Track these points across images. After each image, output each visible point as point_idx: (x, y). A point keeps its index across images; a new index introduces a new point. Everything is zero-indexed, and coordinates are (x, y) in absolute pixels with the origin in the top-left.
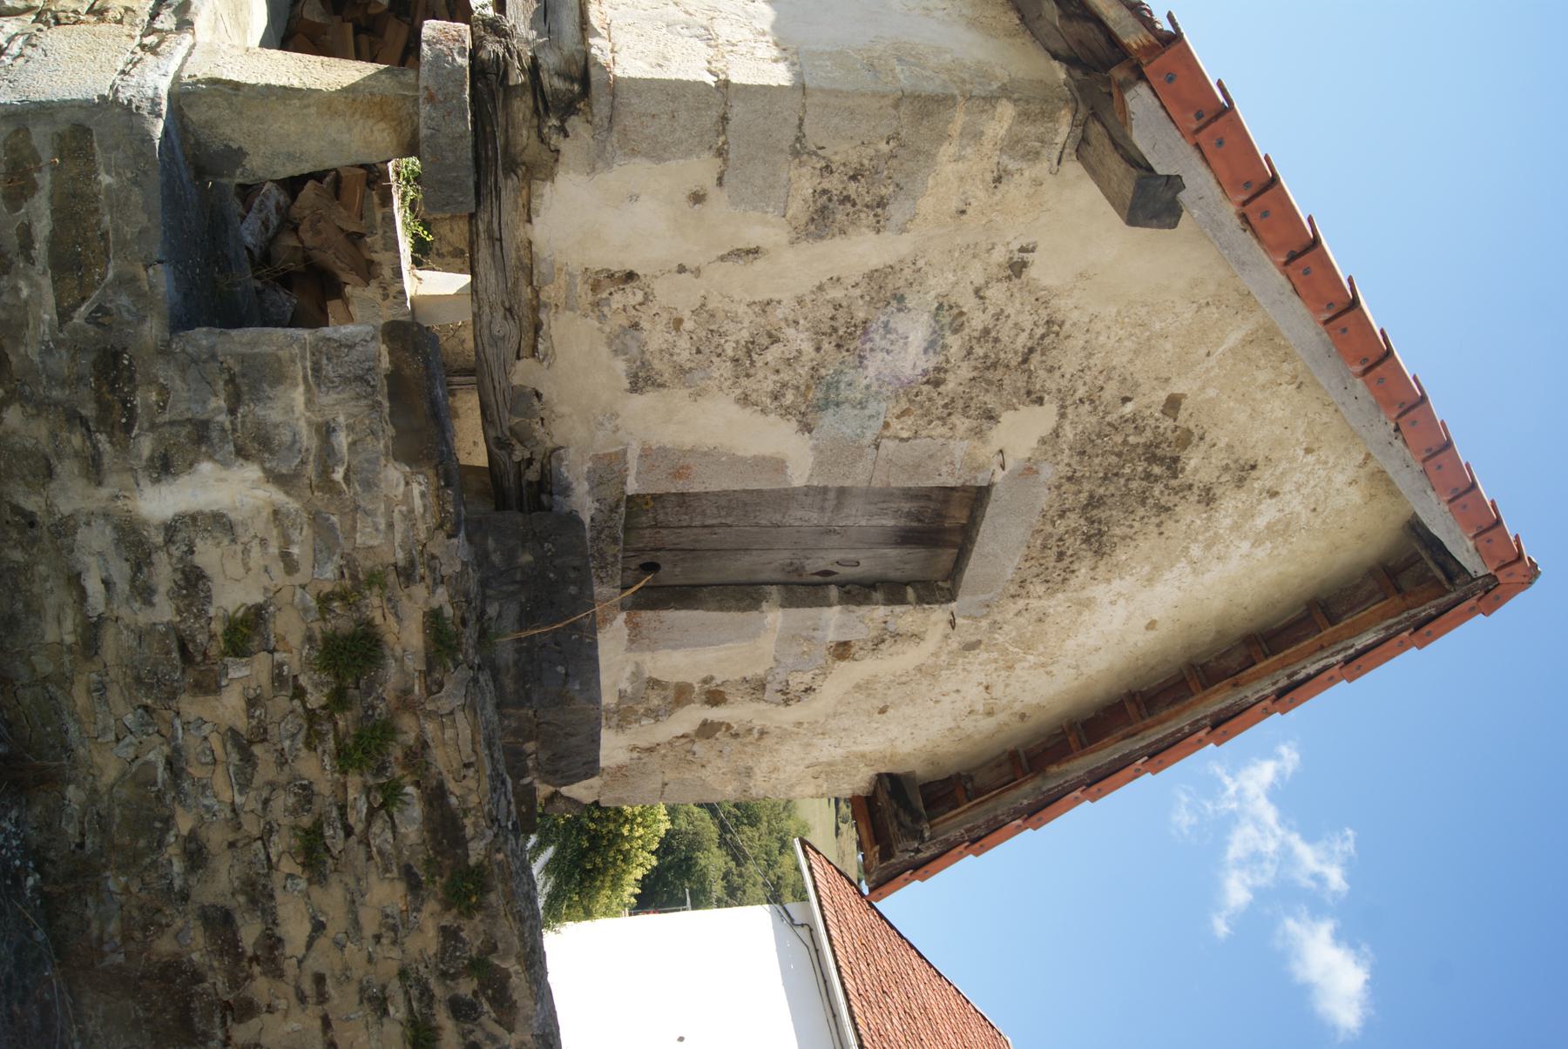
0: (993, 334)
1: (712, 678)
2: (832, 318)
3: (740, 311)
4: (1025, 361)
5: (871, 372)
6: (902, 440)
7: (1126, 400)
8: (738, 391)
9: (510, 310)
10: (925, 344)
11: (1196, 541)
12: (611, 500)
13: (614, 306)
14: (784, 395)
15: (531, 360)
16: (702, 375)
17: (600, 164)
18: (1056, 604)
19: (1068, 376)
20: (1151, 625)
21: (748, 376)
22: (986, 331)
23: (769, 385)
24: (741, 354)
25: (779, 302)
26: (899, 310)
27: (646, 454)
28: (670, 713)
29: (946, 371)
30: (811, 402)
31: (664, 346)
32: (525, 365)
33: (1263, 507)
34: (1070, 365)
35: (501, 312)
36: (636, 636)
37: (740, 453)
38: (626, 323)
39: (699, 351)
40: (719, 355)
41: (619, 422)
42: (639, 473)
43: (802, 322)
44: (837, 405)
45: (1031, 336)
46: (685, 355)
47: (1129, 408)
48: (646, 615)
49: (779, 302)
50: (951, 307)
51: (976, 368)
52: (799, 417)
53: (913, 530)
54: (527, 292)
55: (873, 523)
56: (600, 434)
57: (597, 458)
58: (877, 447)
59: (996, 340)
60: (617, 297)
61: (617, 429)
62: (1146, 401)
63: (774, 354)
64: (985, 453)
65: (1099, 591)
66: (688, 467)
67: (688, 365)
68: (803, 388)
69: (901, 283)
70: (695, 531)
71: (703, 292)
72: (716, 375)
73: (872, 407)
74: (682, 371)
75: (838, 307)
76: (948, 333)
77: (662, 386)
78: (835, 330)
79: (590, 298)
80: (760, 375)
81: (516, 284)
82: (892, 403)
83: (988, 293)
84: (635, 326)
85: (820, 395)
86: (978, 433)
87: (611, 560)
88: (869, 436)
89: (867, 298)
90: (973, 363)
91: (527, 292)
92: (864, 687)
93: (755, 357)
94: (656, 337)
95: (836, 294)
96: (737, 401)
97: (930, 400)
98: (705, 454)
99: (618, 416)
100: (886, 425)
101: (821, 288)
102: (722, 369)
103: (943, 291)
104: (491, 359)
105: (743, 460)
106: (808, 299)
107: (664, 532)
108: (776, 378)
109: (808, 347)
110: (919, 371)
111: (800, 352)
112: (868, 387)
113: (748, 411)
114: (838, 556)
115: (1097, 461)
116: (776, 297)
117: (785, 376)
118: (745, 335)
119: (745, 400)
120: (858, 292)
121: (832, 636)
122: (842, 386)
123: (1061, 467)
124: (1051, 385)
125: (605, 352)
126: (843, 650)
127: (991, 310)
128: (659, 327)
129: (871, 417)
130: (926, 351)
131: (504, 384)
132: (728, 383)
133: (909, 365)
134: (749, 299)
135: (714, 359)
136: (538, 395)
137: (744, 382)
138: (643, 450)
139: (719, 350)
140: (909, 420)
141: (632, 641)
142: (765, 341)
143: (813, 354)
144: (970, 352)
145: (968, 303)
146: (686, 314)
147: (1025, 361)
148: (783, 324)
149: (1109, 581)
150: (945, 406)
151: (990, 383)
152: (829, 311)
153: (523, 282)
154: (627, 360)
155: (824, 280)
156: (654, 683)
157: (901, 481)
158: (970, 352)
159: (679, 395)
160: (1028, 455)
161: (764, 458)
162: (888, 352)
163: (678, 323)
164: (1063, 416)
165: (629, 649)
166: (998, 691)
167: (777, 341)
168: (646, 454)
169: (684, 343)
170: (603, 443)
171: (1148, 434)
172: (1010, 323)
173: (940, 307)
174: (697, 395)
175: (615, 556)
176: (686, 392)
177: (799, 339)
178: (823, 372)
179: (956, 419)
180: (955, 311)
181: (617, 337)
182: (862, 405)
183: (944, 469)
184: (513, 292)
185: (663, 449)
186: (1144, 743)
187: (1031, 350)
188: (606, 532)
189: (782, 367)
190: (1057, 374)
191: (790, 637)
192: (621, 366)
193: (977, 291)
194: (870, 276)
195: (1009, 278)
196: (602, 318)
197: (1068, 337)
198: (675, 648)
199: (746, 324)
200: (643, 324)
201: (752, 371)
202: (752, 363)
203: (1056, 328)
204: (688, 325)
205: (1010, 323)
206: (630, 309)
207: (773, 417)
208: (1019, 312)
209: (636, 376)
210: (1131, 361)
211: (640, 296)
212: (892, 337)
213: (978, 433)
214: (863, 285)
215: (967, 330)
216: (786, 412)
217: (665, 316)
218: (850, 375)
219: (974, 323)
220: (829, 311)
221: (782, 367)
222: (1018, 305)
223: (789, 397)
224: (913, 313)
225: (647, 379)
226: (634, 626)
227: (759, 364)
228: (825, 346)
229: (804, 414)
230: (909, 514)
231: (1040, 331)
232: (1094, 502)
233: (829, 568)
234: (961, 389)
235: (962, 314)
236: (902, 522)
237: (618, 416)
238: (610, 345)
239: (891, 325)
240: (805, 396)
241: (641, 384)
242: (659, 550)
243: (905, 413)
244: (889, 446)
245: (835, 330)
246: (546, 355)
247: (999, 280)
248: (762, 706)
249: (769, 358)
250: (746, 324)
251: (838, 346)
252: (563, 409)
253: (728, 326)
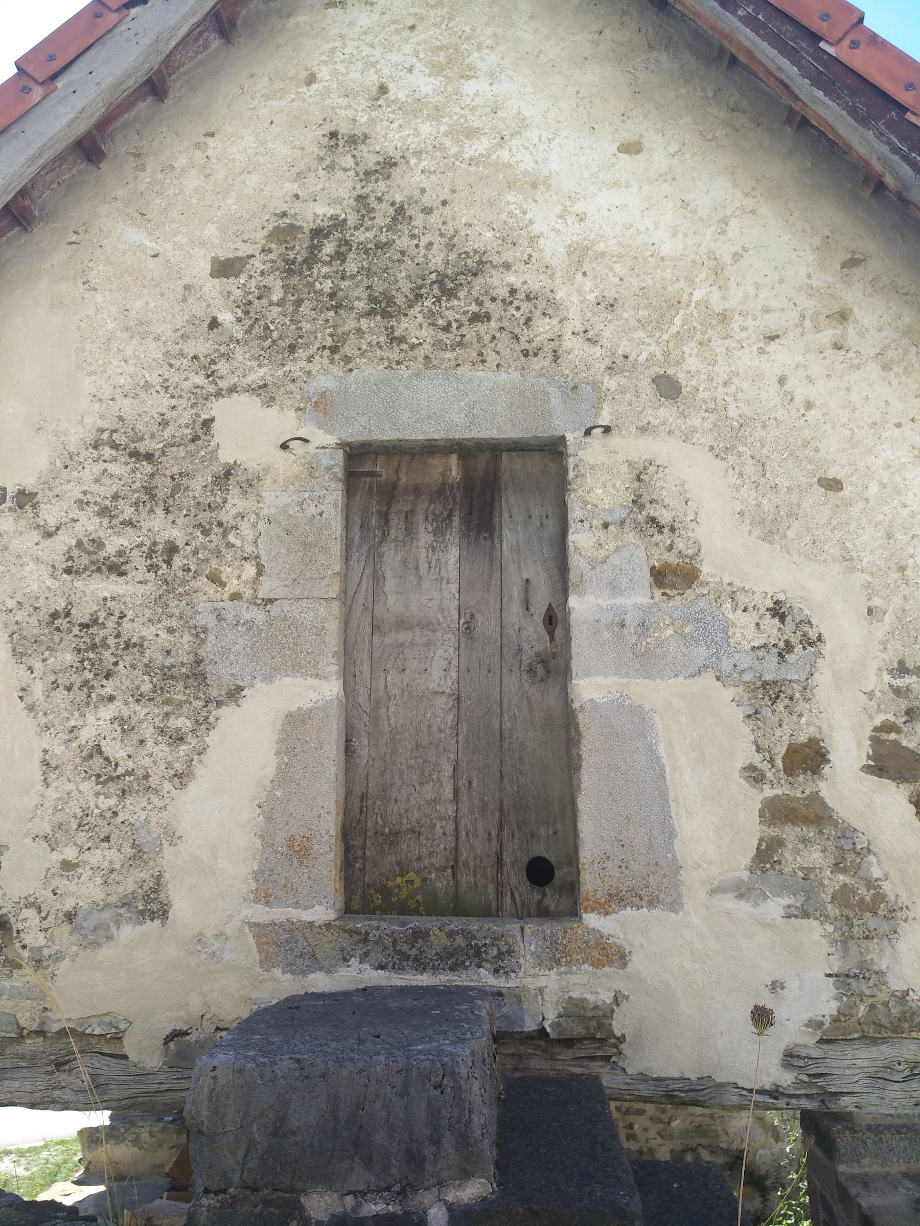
0: (107, 503)
1: (751, 768)
2: (69, 689)
3: (56, 795)
4: (149, 457)
5: (149, 632)
6: (260, 573)
7: (214, 324)
8: (167, 786)
9: (59, 1065)
10: (113, 577)
11: (458, 156)
12: (345, 941)
13: (43, 942)
14: (177, 730)
15: (125, 1041)
16: (143, 833)
17: (8, 925)
18: (575, 297)
19: (173, 402)
20: (631, 148)
21: (146, 777)
22: (104, 512)
23: (162, 750)
24: (113, 788)
25: (45, 751)
26: (68, 614)
27: (263, 897)
28: (847, 832)
29: (155, 544)
30: (193, 687)
31: (99, 880)
32: (129, 1047)
33: (402, 96)
34: (160, 403)
35: (61, 1076)
36: (653, 889)
37: (271, 772)
38: (66, 928)
39: (107, 839)
40: (115, 814)
41: (209, 934)
42: (297, 905)
43: (73, 723)
44: (198, 662)
45: (115, 460)
46: (113, 854)
47: (226, 317)
48: (589, 882)
49: (45, 751)
50: (70, 558)
51: (152, 511)
52: (211, 707)
53: (466, 522)
54: (30, 1045)
55: (453, 575)
56: (228, 957)
57: (267, 963)
58: (271, 601)
59: (116, 497)
60: (28, 939)
61: (220, 935)
62: (219, 301)
63: (115, 750)
64: (286, 466)
65: (553, 248)
66: (292, 839)
67: (128, 851)
68: (167, 708)
69: (33, 621)
70: (464, 809)
71: (28, 840)
72: (143, 815)
73: (206, 619)
74: (139, 855)
75: (55, 685)
76: (103, 554)
77: (158, 879)
78: (86, 683)
79: (28, 970)
80: (147, 762)
81: (22, 1057)
82: (199, 598)
83: (52, 522)
84: (70, 917)
85: (180, 686)
86: (250, 485)
87: (460, 940)
88: (258, 615)
89: (47, 654)
90: (144, 515)
91: (30, 1045)
92: (770, 529)
93: (120, 770)
94: (86, 891)
95: (38, 690)
96: (183, 786)
97: (196, 553)
98: (269, 819)
99: (201, 934)
100: (236, 597)
101: (31, 708)
102: (135, 809)
103: (45, 572)
104: (126, 1093)
105: (282, 771)
106: (43, 720)
107: (464, 854)
108: (150, 744)
109: (107, 712)
110: (151, 576)
111: (113, 721)
112: (171, 630)
113: (199, 770)
114: (515, 609)
115: (306, 326)
116: (38, 756)
117: (148, 731)
118: (88, 787)
119: (182, 778)
120: (38, 666)
121: (639, 596)
122: (170, 661)
123: (314, 367)
124: (186, 417)
125: (105, 952)
126: (673, 577)
127: (76, 513)
128: (73, 888)
129: (220, 618)
130: (123, 574)
131: (162, 1078)
132: (155, 800)
133: (140, 589)
134: (39, 787)
135: (120, 819)
136: (176, 1035)
137: (154, 781)
138: (257, 900)
139: (108, 814)
140: (226, 572)
141: (653, 902)
142: (97, 762)
143: (117, 703)
144: (130, 523)
145: (65, 540)
146: (56, 857)
147: (149, 457)
148: (75, 744)
149: (533, 239)
150: (206, 533)
151: (175, 490)
152: (61, 694)
153: (19, 1049)
154: (118, 924)
155: (23, 705)
156: (766, 855)
157: (332, 559)
158: (130, 523)
159: (171, 858)
160: (292, 413)
161: (282, 741)
162: (122, 616)
163: (67, 865)
164: (233, 390)
165: (675, 906)
166: (771, 322)
167: (98, 750)
168: (263, 897)
169: (95, 858)
170: (244, 951)
171: (269, 280)
172: (95, 488)
173: (68, 571)
174: (173, 837)
175: (451, 935)
176: (167, 850)
177: (97, 724)
178: (146, 687)
179: (227, 516)
180: (75, 553)
181: (85, 937)
182: (199, 634)
183: (312, 510)
184: (33, 1061)
185: (257, 876)
186: (784, 63)
187: (135, 454)
188: (405, 948)
189: (135, 738)
190: (170, 414)
191: (646, 661)
192: (127, 932)
193: (48, 535)
194: (18, 655)
195: (34, 507)
196: (58, 957)
197: (121, 419)
198: (670, 834)
199: (72, 787)
200: (69, 905)
201: (140, 772)
202: (129, 773)
203: (105, 436)
204: (70, 854)
205: (95, 488)
206: (45, 924)
207: (211, 739)
208: (80, 481)
209: (142, 913)
210: (157, 339)
211: (30, 913)
212: (102, 615)
213: (250, 485)
214: (31, 661)
215: (101, 534)
216: (204, 723)
217: (56, 882)
218: (154, 654)
219: (91, 528)
220: (61, 694)
221: (135, 738)
222: (70, 486)
223: (181, 722)
224: (73, 599)
225: (147, 899)
226: (614, 901)
227: (130, 765)
228: (109, 690)
229: (208, 702)
230: (438, 532)
231: (107, 452)
232: (383, 307)
233: (539, 618)
234: (180, 521)
235: (79, 544)
236: (453, 537)
237: (201, 934)
238: (96, 944)
239: (86, 620)
240: (180, 705)
241: (155, 907)
242: (500, 860)
243: (215, 579)
244: (267, 588)
245: (86, 683)
246: (111, 1024)
247: (37, 515)
248: (824, 679)
249: (122, 754)
250: (72, 787)
251: (108, 676)
252: (195, 1005)
253: (74, 807)
